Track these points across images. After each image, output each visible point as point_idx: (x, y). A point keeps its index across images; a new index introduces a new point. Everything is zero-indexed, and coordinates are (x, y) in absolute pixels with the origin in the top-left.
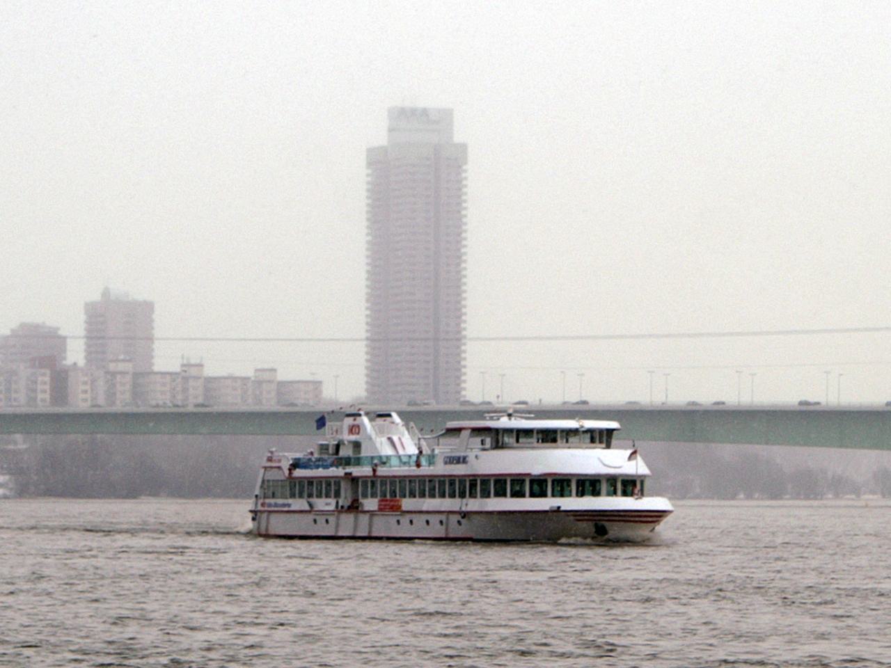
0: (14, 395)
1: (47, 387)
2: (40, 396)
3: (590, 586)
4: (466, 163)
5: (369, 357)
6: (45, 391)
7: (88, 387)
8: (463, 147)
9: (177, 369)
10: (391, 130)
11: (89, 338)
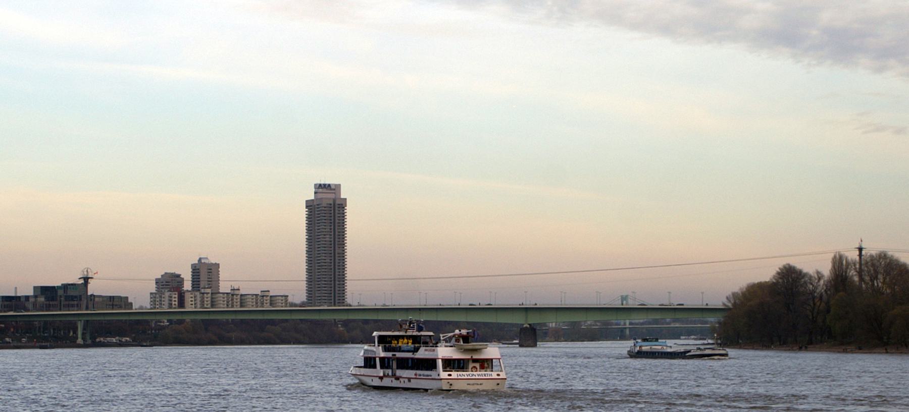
0: (163, 303)
1: (177, 299)
2: (173, 303)
3: (576, 371)
4: (346, 206)
5: (307, 285)
6: (175, 301)
7: (163, 303)
9: (229, 291)
10: (315, 193)
11: (193, 281)
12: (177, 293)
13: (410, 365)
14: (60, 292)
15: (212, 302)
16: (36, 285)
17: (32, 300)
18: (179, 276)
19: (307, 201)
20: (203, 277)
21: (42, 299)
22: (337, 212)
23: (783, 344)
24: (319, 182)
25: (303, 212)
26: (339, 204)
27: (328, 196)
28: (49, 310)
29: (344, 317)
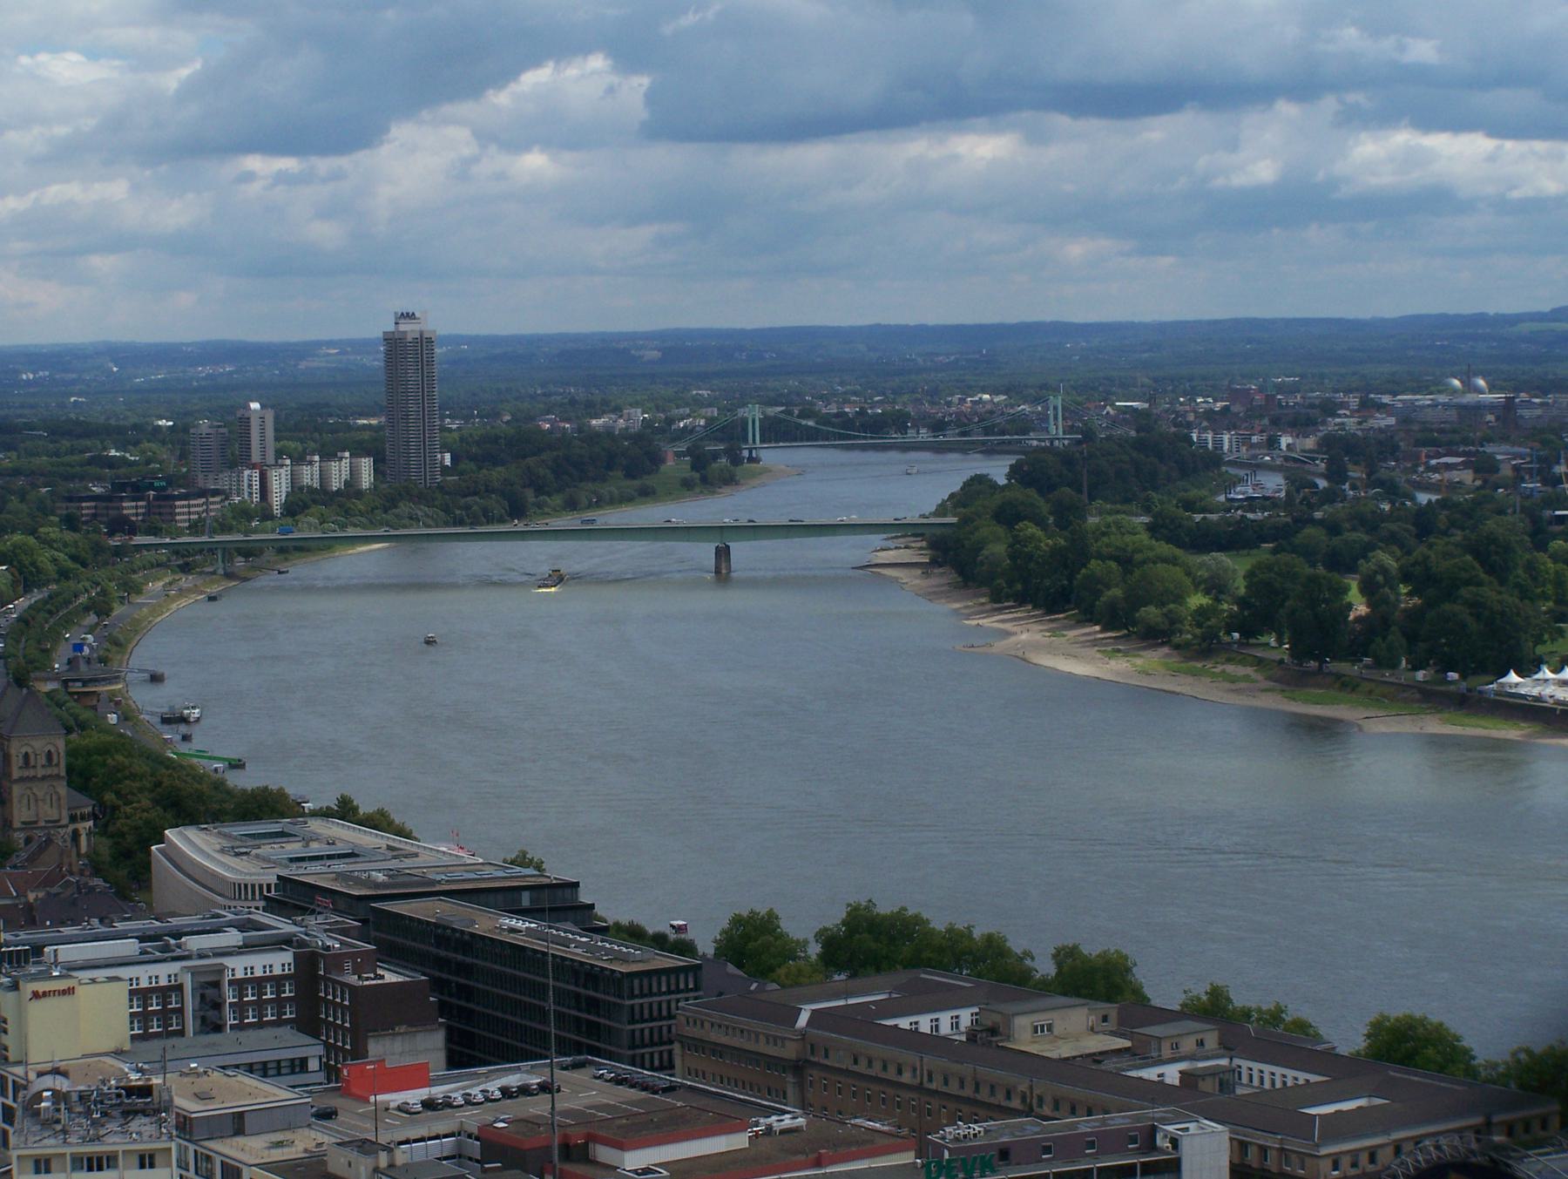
2: (254, 483)
12: (257, 471)
22: (425, 348)
23: (203, 996)
26: (427, 338)
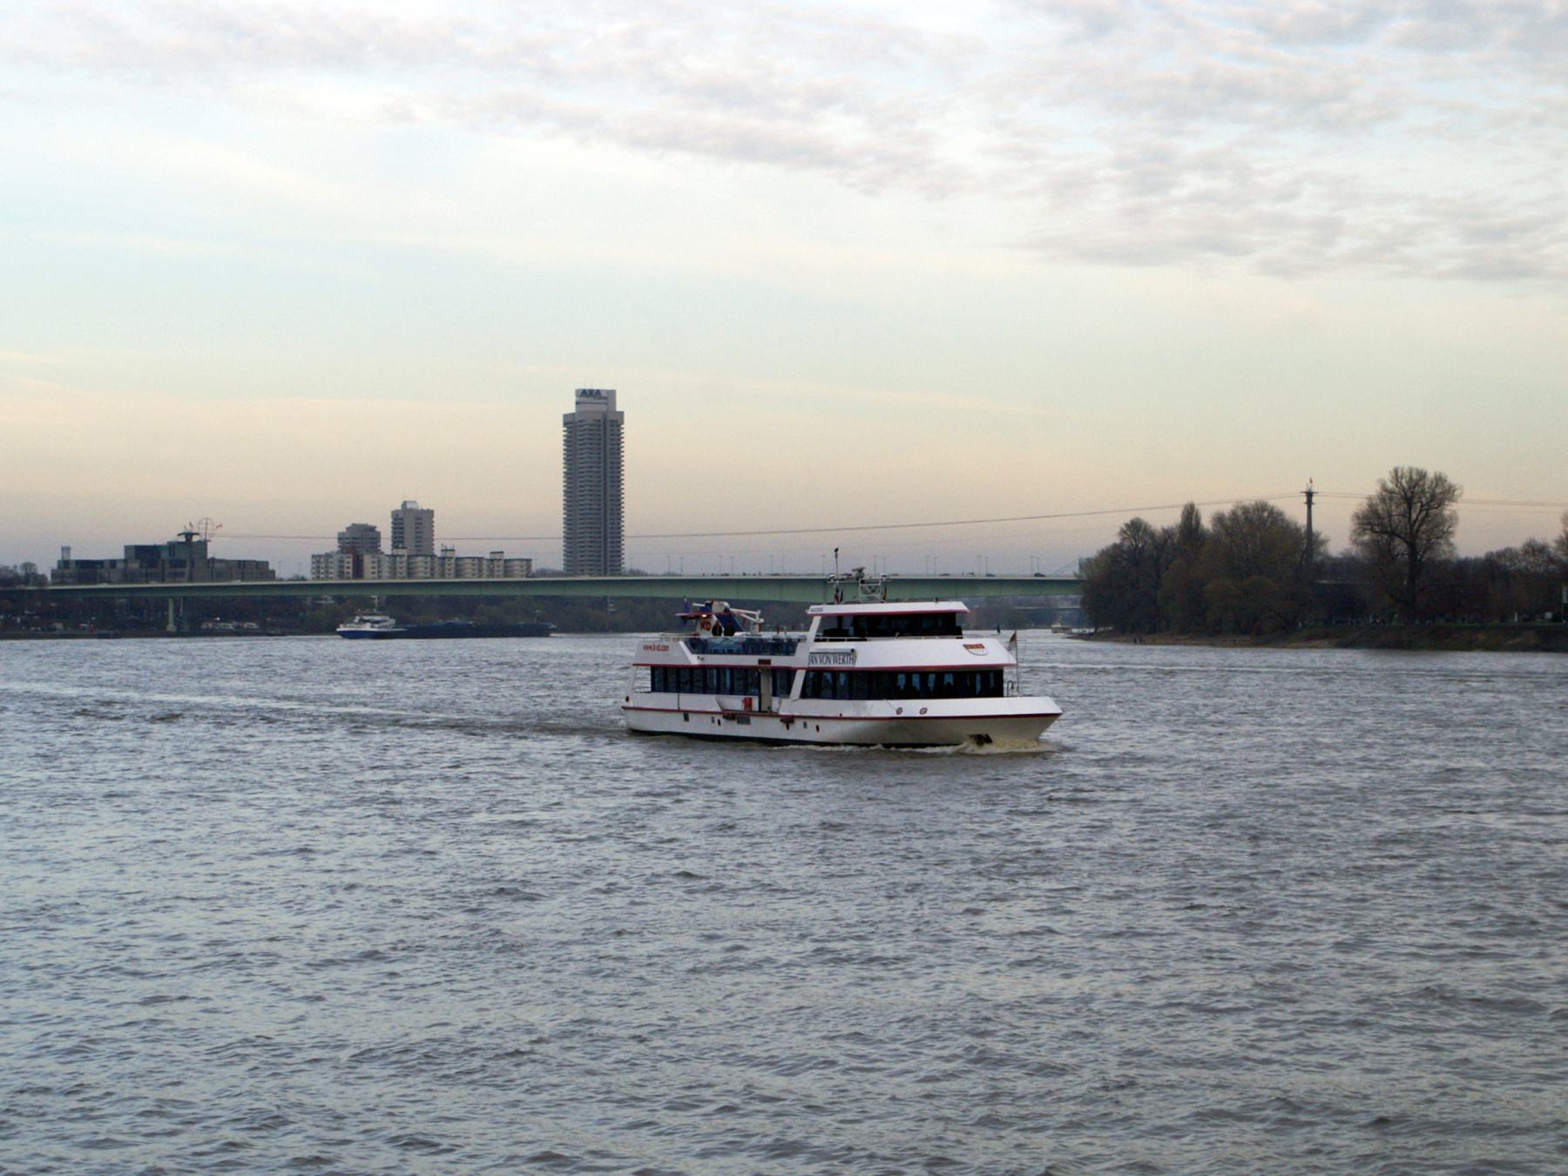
8: (622, 414)
10: (577, 403)
13: (978, 677)
14: (165, 555)
15: (408, 568)
16: (128, 544)
17: (120, 566)
18: (372, 529)
19: (565, 416)
20: (409, 533)
21: (135, 565)
24: (583, 387)
25: (558, 434)
27: (598, 408)
28: (262, 580)
29: (278, 593)
